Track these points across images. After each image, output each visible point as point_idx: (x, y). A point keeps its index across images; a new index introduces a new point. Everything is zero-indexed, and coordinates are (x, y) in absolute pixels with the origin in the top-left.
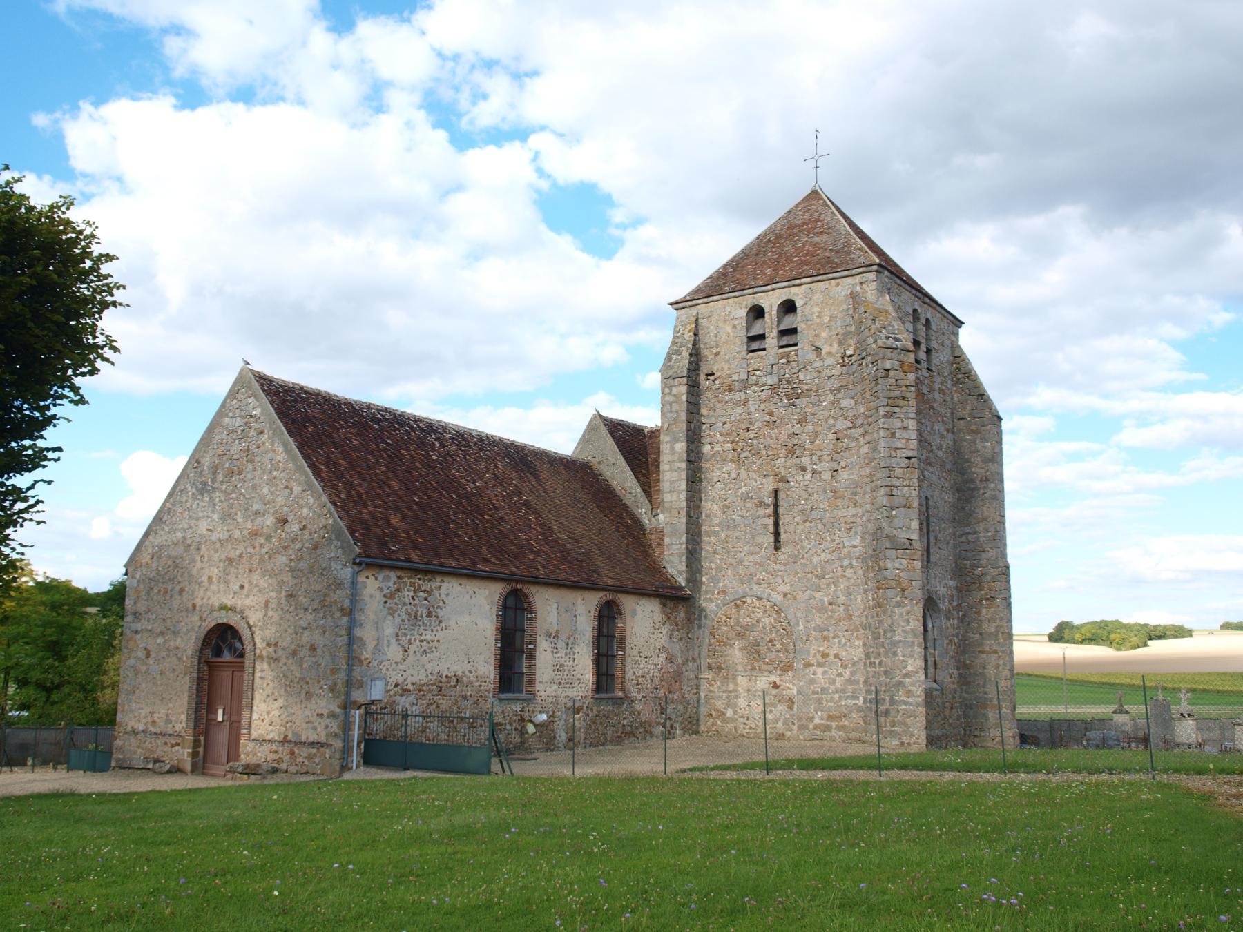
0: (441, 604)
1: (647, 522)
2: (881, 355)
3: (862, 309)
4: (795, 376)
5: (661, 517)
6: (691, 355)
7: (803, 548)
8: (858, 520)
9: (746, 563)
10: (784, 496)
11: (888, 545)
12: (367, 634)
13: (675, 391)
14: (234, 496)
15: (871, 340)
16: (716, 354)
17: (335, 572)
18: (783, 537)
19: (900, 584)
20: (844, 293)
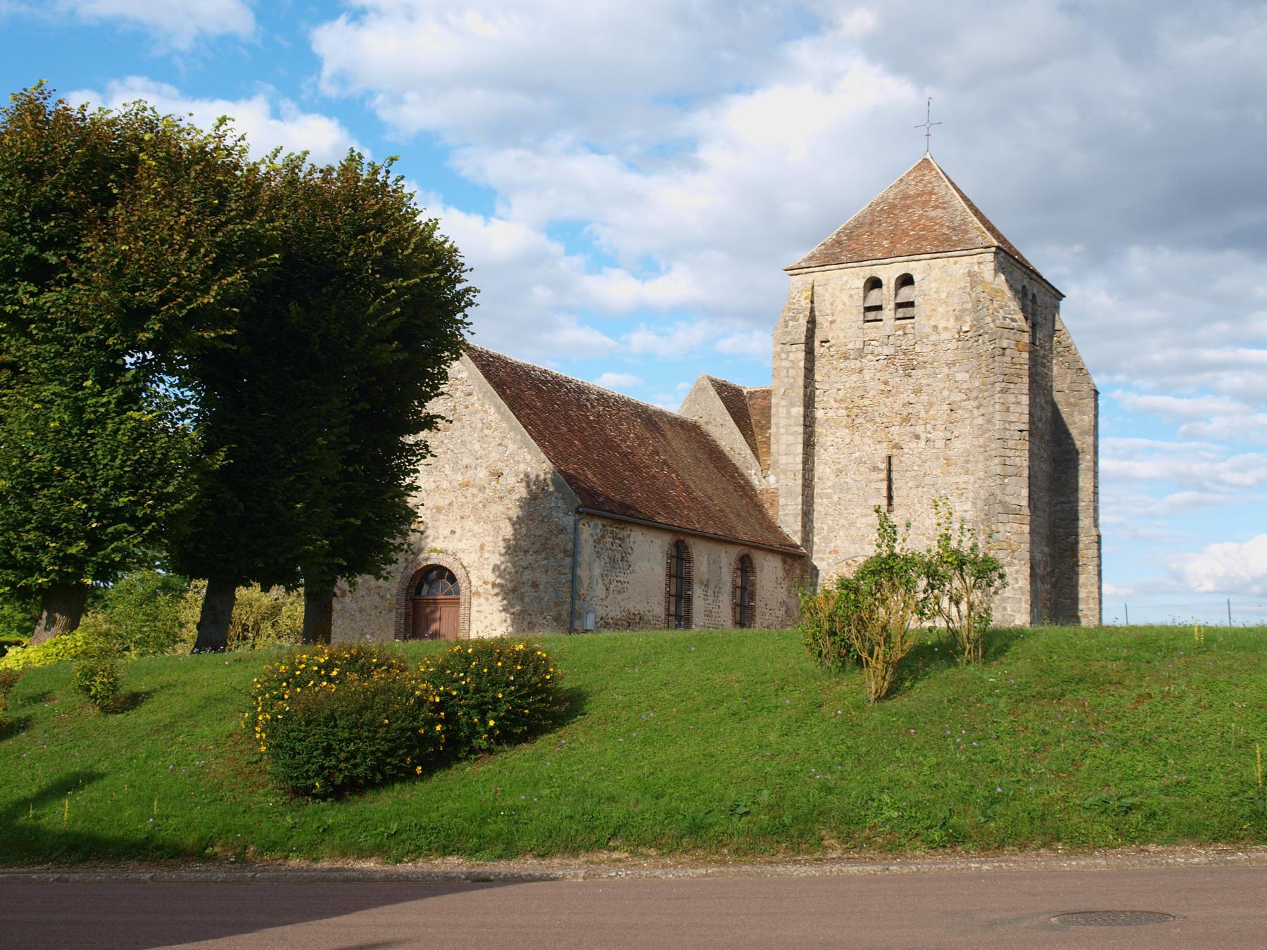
0: (630, 551)
1: (757, 483)
2: (999, 334)
3: (979, 289)
4: (912, 347)
5: (772, 479)
6: (808, 322)
7: (915, 511)
8: (970, 487)
9: (859, 525)
10: (898, 462)
11: (1000, 510)
12: (583, 573)
13: (792, 356)
15: (989, 319)
16: (832, 322)
17: (556, 520)
18: (896, 501)
19: (1011, 545)
20: (962, 271)
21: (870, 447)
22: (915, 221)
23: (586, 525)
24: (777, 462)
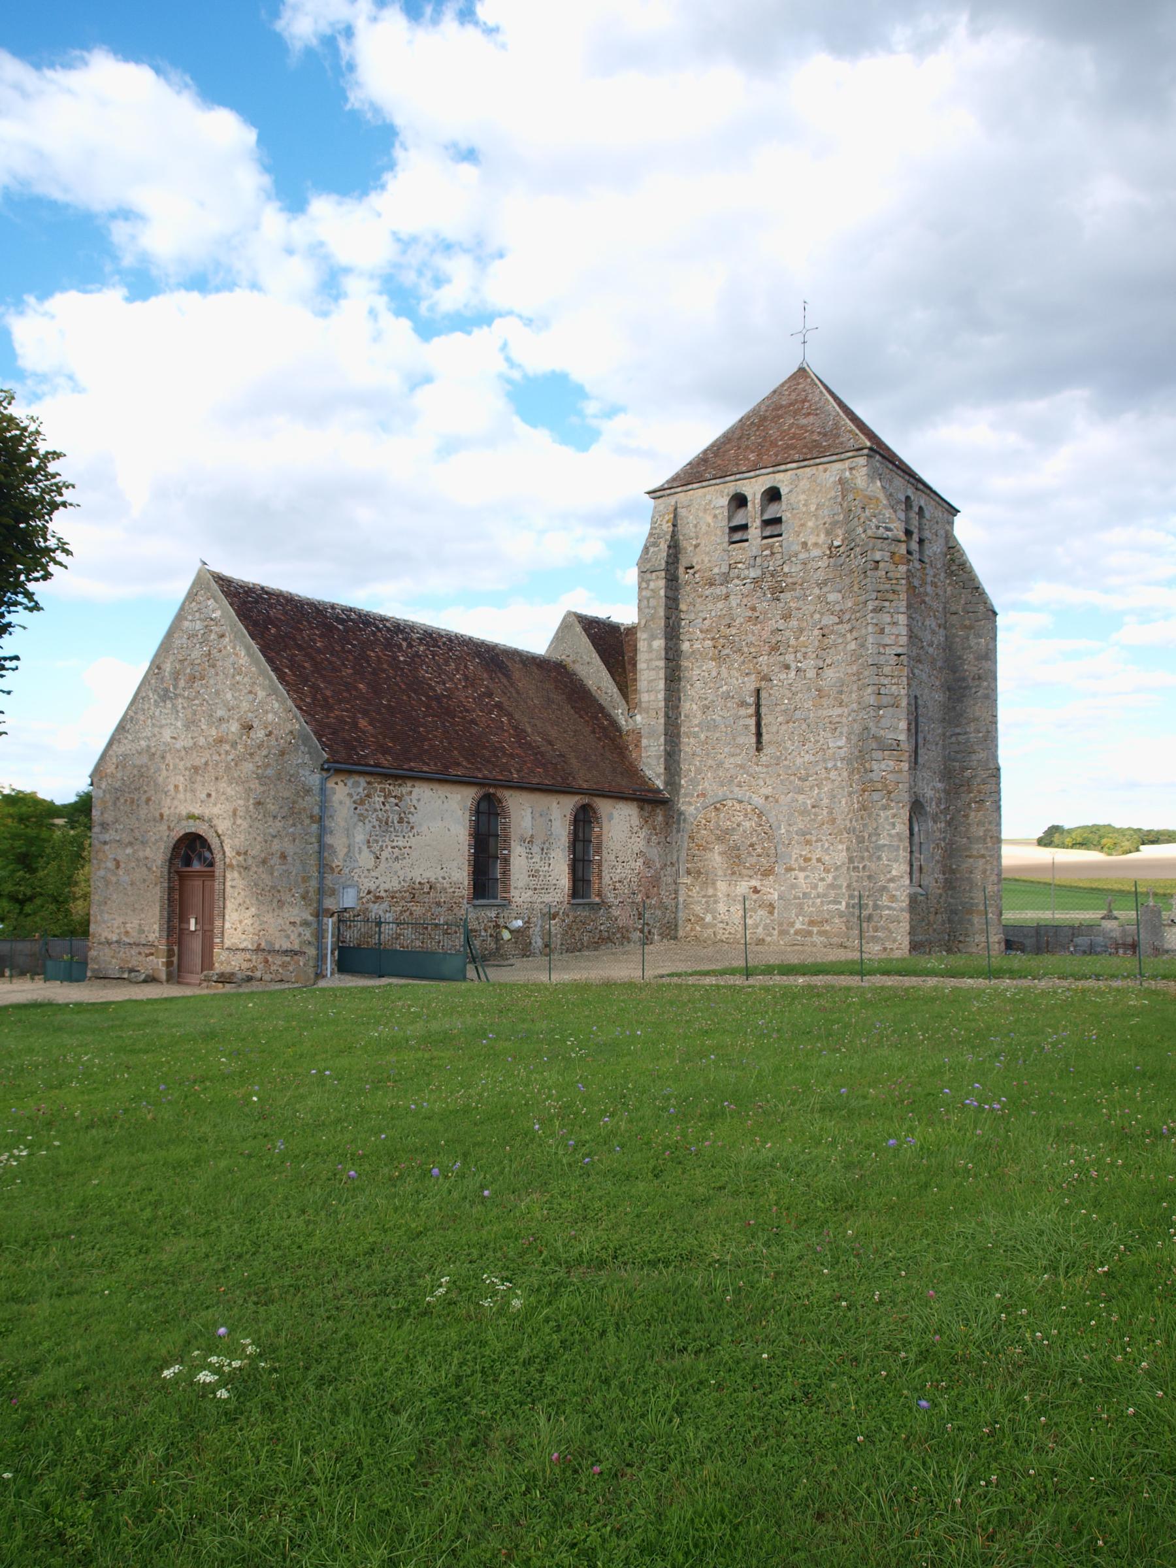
0: (412, 810)
1: (624, 723)
2: (871, 545)
3: (850, 497)
6: (669, 547)
7: (786, 749)
8: (844, 720)
11: (874, 746)
12: (337, 841)
13: (652, 585)
14: (197, 702)
15: (860, 530)
16: (696, 546)
17: (303, 778)
19: (886, 786)
20: (832, 479)
21: (737, 680)
22: (785, 431)
23: (340, 783)
24: (640, 702)
